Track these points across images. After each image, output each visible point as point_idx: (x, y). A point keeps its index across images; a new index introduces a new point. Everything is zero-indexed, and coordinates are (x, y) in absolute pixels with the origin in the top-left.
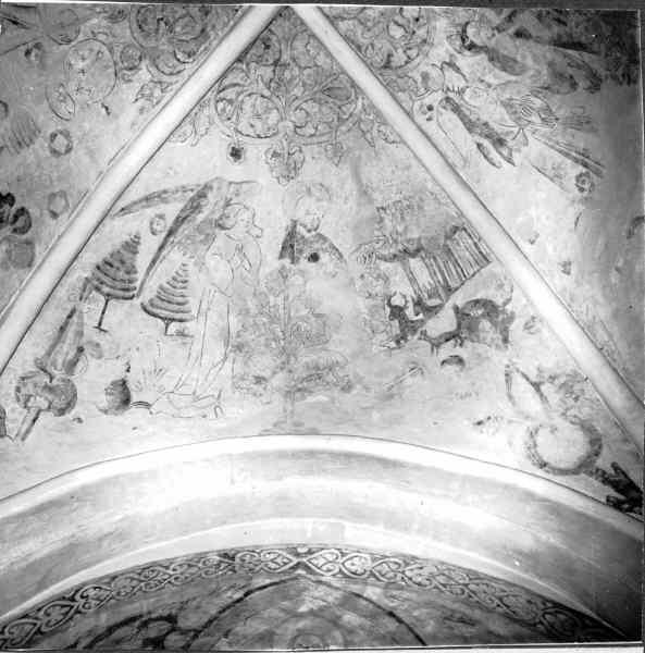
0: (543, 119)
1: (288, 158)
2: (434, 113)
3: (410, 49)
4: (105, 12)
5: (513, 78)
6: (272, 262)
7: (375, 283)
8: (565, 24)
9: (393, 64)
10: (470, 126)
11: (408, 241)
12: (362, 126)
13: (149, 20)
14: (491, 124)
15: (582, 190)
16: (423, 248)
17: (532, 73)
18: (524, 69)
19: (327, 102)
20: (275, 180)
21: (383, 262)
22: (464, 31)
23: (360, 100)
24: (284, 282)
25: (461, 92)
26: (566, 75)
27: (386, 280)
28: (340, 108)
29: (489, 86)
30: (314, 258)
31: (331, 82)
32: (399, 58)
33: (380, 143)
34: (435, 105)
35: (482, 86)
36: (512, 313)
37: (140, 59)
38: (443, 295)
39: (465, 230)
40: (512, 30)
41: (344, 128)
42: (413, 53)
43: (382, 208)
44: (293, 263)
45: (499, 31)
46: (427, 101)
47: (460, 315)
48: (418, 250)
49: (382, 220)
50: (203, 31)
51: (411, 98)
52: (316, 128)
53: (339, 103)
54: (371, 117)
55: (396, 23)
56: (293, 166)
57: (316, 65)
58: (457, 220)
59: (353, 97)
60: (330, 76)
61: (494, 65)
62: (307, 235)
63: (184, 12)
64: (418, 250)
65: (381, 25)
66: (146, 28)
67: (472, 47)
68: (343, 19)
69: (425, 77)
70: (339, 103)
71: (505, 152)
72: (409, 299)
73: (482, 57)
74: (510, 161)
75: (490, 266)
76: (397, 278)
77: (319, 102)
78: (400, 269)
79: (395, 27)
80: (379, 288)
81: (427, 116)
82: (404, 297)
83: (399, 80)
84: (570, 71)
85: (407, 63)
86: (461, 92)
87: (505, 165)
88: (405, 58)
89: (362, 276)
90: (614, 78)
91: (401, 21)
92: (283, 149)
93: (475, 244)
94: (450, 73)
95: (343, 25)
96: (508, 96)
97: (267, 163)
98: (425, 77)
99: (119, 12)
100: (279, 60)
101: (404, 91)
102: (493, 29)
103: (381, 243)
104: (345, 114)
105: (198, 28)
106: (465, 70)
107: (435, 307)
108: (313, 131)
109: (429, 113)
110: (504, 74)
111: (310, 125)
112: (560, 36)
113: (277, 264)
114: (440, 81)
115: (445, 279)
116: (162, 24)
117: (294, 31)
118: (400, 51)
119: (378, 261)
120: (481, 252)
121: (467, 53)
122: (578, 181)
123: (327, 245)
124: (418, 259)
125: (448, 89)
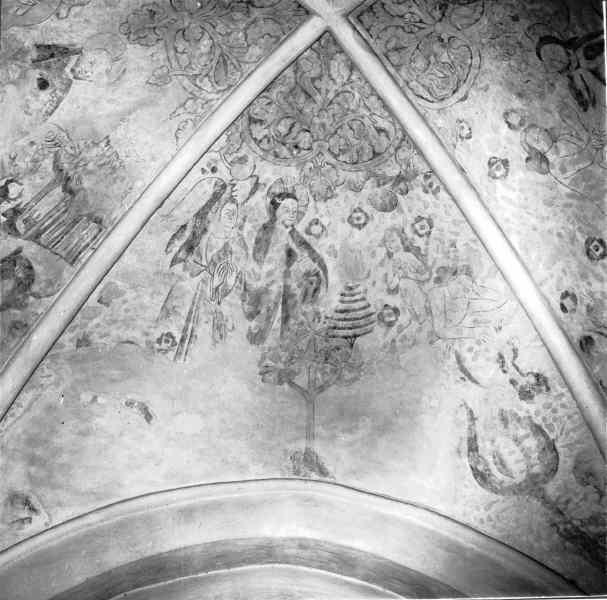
0: (217, 289)
1: (150, 28)
2: (210, 175)
5: (251, 252)
6: (28, 39)
7: (28, 159)
8: (303, 301)
9: (253, 126)
10: (202, 215)
11: (79, 179)
12: (190, 103)
14: (208, 235)
15: (159, 341)
16: (74, 196)
17: (257, 270)
18: (259, 261)
19: (212, 60)
20: (124, 20)
21: (52, 160)
22: (289, 196)
23: (217, 96)
24: (10, 59)
25: (232, 200)
26: (259, 308)
27: (33, 171)
28: (207, 75)
29: (241, 228)
30: (43, 84)
32: (259, 132)
33: (175, 124)
34: (217, 175)
35: (240, 220)
36: (27, 305)
38: (30, 233)
39: (100, 230)
40: (294, 246)
41: (186, 82)
42: (265, 145)
43: (109, 141)
44: (33, 62)
45: (290, 232)
46: (222, 167)
47: (12, 257)
48: (71, 192)
49: (96, 144)
52: (183, 53)
53: (211, 74)
54: (200, 110)
55: (293, 126)
56: (142, 35)
57: (249, 46)
58: (108, 221)
59: (219, 88)
60: (238, 61)
61: (260, 230)
62: (67, 70)
64: (71, 192)
67: (274, 205)
68: (295, 72)
69: (243, 160)
70: (211, 74)
71: (182, 255)
72: (19, 200)
73: (265, 218)
74: (174, 262)
75: (68, 266)
76: (38, 181)
78: (49, 180)
80: (23, 164)
81: (206, 168)
82: (20, 195)
83: (238, 135)
84: (263, 311)
85: (255, 139)
86: (232, 200)
87: (171, 256)
88: (259, 138)
89: (32, 143)
90: (264, 358)
91: (295, 129)
92: (160, 21)
93: (88, 245)
94: (248, 185)
95: (289, 72)
96: (234, 249)
97: (143, 6)
100: (253, 6)
102: (292, 226)
103: (72, 152)
104: (201, 81)
106: (252, 201)
107: (15, 229)
108: (179, 50)
109: (209, 170)
110: (253, 241)
111: (187, 44)
112: (294, 295)
113: (28, 43)
114: (239, 176)
115: (46, 229)
117: (282, 20)
118: (266, 132)
119: (52, 155)
120: (80, 253)
121: (269, 200)
122: (167, 335)
123: (59, 94)
124: (62, 194)
125: (234, 185)
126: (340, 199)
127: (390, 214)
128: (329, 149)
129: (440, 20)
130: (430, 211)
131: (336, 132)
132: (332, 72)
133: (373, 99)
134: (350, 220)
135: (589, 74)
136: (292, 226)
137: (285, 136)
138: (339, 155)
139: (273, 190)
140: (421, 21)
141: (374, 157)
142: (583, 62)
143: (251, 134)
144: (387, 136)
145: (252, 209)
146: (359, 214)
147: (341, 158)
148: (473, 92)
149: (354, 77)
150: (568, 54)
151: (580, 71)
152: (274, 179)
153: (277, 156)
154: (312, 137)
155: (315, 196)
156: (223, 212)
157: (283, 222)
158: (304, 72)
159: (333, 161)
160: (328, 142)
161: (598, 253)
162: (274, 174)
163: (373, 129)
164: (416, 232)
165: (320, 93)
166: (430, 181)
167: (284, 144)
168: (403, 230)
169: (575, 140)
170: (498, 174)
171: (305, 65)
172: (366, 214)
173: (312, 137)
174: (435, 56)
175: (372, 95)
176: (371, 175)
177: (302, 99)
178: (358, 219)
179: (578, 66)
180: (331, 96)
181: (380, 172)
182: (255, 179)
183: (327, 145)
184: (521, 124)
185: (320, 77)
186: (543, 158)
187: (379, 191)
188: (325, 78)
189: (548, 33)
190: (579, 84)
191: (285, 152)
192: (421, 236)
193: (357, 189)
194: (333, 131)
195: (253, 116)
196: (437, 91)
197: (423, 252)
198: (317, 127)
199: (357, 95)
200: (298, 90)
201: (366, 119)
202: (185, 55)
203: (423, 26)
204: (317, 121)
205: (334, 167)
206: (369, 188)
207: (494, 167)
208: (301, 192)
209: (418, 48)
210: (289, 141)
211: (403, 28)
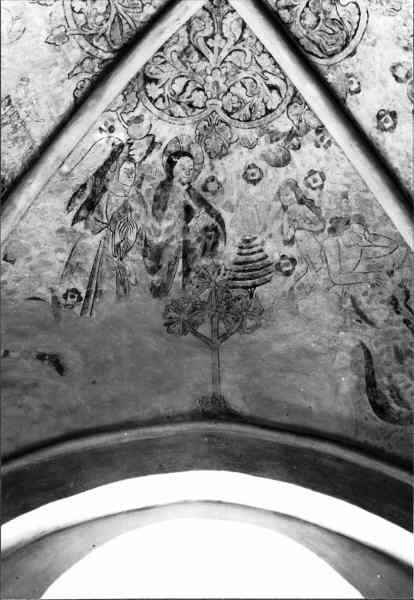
3: (164, 101)
9: (148, 86)
31: (127, 23)
32: (154, 90)
41: (83, 42)
42: (160, 104)
46: (117, 125)
51: (119, 108)
52: (80, 12)
53: (108, 33)
55: (187, 84)
67: (171, 164)
77: (108, 12)
81: (103, 127)
83: (134, 94)
86: (130, 159)
91: (189, 89)
98: (139, 119)
101: (125, 99)
104: (98, 41)
106: (149, 160)
118: (161, 91)
121: (165, 158)
125: (132, 144)
128: (223, 108)
130: (322, 164)
131: (229, 90)
132: (224, 31)
133: (265, 56)
134: (245, 176)
143: (147, 93)
144: (279, 93)
145: (150, 167)
147: (236, 116)
152: (171, 136)
154: (206, 95)
155: (209, 154)
156: (121, 173)
159: (227, 119)
164: (309, 185)
165: (212, 51)
167: (179, 103)
170: (387, 126)
175: (263, 52)
177: (196, 56)
178: (253, 175)
180: (224, 54)
181: (271, 129)
182: (151, 138)
183: (220, 103)
185: (212, 36)
187: (273, 146)
188: (218, 37)
191: (178, 110)
192: (314, 189)
193: (251, 147)
194: (226, 89)
195: (148, 75)
198: (211, 85)
202: (82, 15)
204: (210, 79)
206: (263, 145)
207: (383, 120)
209: (307, 6)
210: (183, 99)
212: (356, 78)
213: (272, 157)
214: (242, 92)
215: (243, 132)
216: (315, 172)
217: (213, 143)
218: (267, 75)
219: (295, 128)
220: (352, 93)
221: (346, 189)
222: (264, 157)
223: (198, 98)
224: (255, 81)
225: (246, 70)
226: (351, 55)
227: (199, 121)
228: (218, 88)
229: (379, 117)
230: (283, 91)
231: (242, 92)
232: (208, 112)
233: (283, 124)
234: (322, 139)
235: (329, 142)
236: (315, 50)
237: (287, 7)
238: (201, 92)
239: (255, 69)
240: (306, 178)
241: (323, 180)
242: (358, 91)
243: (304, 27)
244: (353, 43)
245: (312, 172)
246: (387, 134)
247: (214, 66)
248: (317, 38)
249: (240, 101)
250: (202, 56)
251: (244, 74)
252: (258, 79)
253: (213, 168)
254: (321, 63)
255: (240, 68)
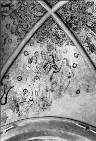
4: (93, 16)
13: (83, 11)
37: (87, 3)
50: (71, 5)
55: (26, 5)
63: (75, 10)
65: (30, 4)
66: (84, 9)
67: (7, 5)
79: (26, 5)
91: (25, 6)
99: (90, 15)
105: (73, 6)
116: (81, 9)
121: (8, 4)
126: (11, 21)
127: (11, 33)
128: (21, 15)
129: (52, 35)
130: (14, 42)
131: (25, 15)
132: (39, 12)
133: (34, 23)
134: (7, 24)
135: (50, 67)
136: (3, 11)
137: (23, 4)
138: (20, 17)
139: (11, 4)
140: (52, 31)
141: (21, 25)
142: (51, 65)
144: (26, 28)
146: (9, 26)
147: (20, 18)
148: (39, 44)
149: (38, 17)
150: (52, 62)
151: (50, 65)
152: (13, 4)
153: (19, 3)
154: (24, 10)
155: (11, 14)
157: (4, 9)
158: (38, 6)
159: (19, 16)
160: (23, 14)
161: (19, 79)
162: (15, 3)
163: (27, 24)
166: (20, 39)
167: (21, 4)
168: (8, 37)
169: (37, 67)
170: (25, 54)
171: (39, 6)
172: (9, 27)
173: (24, 10)
174: (45, 35)
175: (35, 22)
176: (18, 26)
177: (33, 7)
178: (8, 26)
179: (50, 64)
180: (33, 13)
183: (22, 14)
184: (36, 55)
185: (37, 10)
186: (31, 62)
187: (15, 29)
188: (37, 11)
189: (54, 57)
190: (47, 65)
191: (20, 5)
192: (8, 42)
193: (14, 24)
194: (26, 15)
196: (38, 36)
197: (5, 43)
198: (26, 11)
199: (34, 19)
200: (34, 6)
201: (29, 22)
203: (51, 31)
204: (27, 11)
205: (18, 17)
206: (14, 26)
207: (26, 52)
208: (11, 11)
209: (46, 31)
210: (22, 5)
211: (50, 27)
212: (33, 44)
213: (13, 29)
214: (25, 19)
215: (17, 21)
216: (12, 41)
217: (13, 15)
218: (30, 24)
219: (20, 33)
220: (30, 44)
221: (10, 49)
222: (12, 28)
223: (23, 9)
224: (28, 21)
225: (31, 19)
226: (38, 42)
227: (18, 10)
228: (26, 13)
229: (27, 51)
230: (27, 28)
231: (25, 19)
232: (20, 11)
233: (20, 30)
234: (19, 40)
235: (19, 42)
236: (37, 34)
237: (45, 26)
238: (24, 9)
239: (31, 20)
240: (10, 39)
241: (11, 43)
242: (31, 45)
243: (42, 31)
244: (40, 42)
245: (11, 40)
246: (24, 54)
247: (31, 11)
248: (40, 34)
249: (23, 19)
250: (33, 8)
251: (29, 18)
252: (29, 22)
253: (8, 16)
254: (35, 36)
255: (31, 17)
